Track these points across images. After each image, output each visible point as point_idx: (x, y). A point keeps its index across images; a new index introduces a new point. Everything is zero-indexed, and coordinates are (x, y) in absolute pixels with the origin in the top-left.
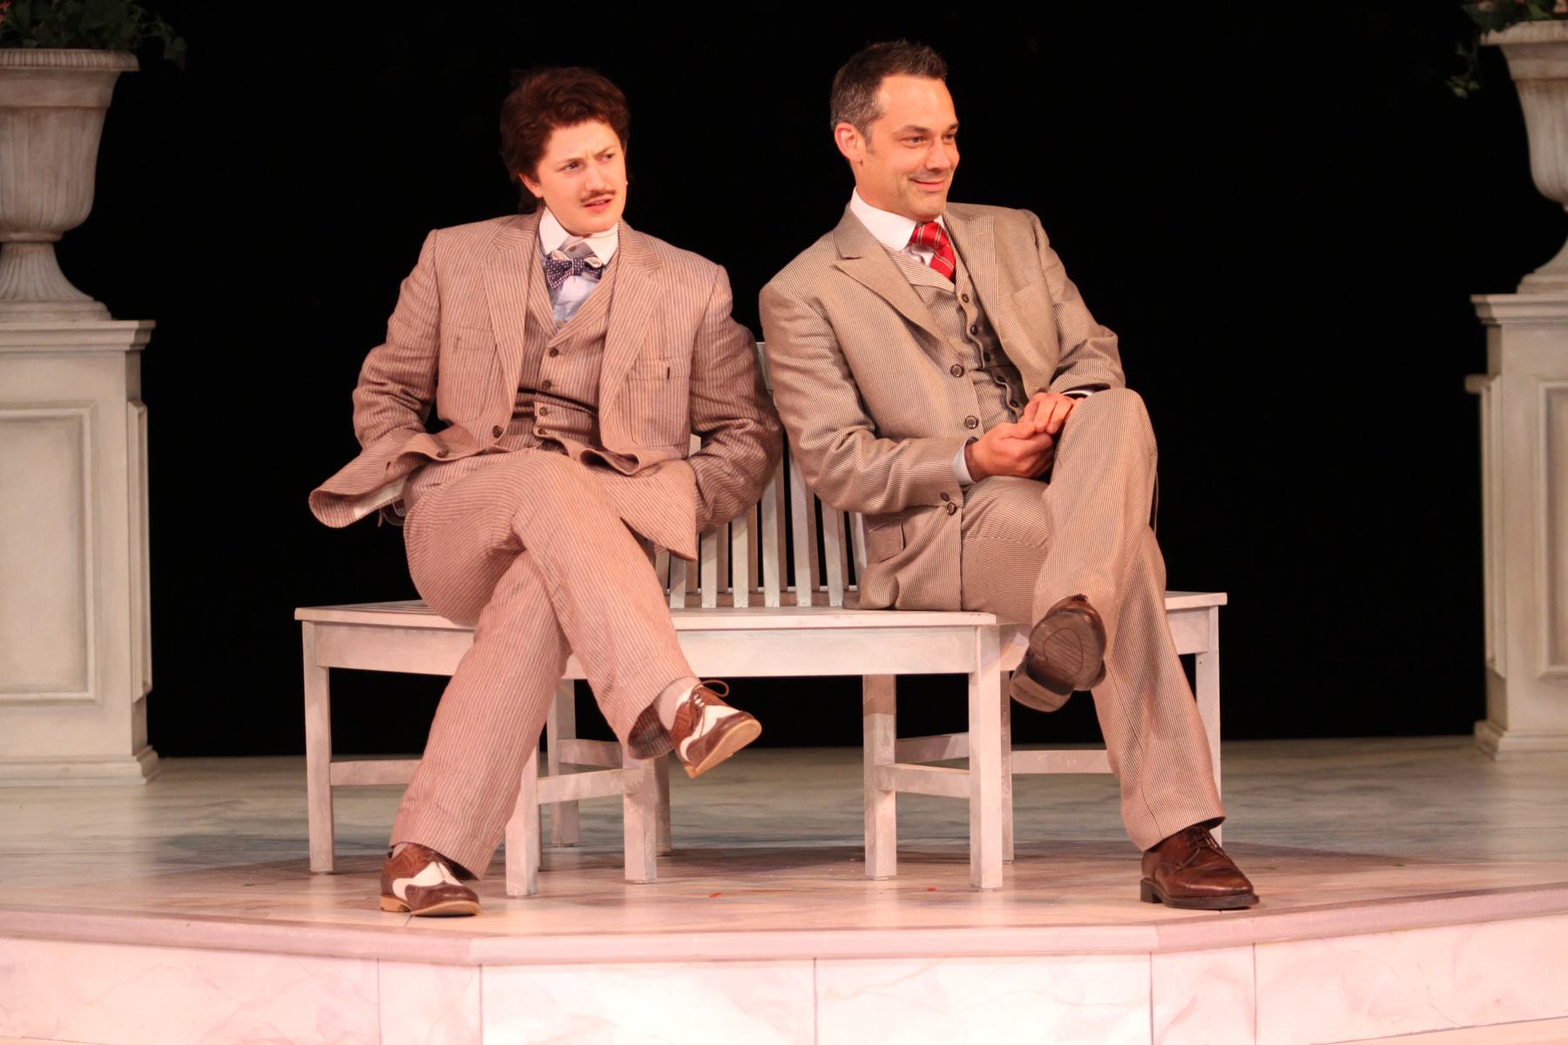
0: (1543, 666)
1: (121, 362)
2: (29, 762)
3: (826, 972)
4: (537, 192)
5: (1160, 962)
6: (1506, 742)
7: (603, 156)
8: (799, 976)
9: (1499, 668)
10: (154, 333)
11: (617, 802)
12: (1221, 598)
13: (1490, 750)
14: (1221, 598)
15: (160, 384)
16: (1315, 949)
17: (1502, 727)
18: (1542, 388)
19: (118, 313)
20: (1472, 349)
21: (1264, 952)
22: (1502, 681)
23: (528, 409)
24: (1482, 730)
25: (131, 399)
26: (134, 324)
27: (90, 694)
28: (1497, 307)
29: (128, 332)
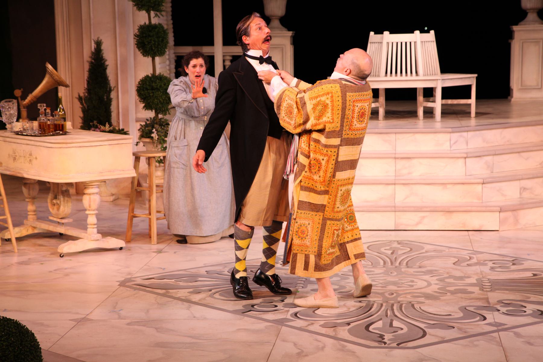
0: (520, 87)
1: (289, 38)
3: (398, 135)
4: (187, 71)
5: (452, 134)
6: (513, 100)
7: (201, 66)
8: (393, 136)
9: (512, 87)
10: (295, 34)
11: (378, 108)
12: (476, 75)
13: (510, 101)
14: (476, 75)
15: (295, 42)
16: (478, 132)
17: (512, 97)
18: (521, 41)
19: (289, 30)
20: (510, 35)
21: (469, 133)
22: (512, 90)
23: (58, 129)
24: (509, 98)
25: (291, 44)
26: (291, 32)
28: (515, 28)
29: (290, 33)
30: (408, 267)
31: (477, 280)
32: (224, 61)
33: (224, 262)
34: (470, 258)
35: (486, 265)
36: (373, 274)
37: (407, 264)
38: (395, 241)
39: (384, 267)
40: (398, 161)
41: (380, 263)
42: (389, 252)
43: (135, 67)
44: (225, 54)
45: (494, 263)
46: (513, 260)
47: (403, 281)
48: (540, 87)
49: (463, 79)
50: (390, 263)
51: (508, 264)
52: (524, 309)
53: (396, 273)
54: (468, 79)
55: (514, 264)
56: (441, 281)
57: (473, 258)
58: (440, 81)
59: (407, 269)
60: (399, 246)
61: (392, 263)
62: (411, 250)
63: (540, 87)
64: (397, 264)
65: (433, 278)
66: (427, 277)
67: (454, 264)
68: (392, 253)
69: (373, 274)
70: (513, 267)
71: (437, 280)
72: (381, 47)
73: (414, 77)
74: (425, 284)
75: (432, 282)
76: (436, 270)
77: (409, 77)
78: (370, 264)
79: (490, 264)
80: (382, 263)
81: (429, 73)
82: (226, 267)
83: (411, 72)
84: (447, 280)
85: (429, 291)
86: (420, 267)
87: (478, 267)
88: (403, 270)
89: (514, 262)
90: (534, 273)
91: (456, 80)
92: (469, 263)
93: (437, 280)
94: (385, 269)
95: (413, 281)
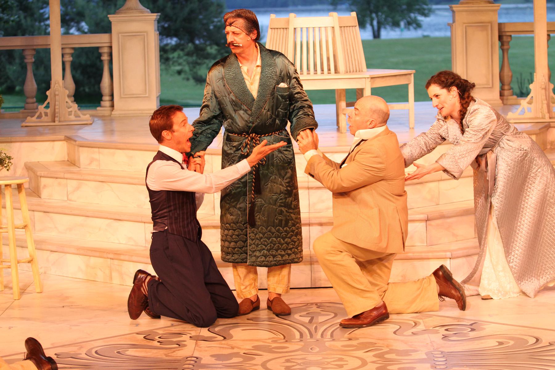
2: (134, 110)
10: (160, 16)
19: (152, 12)
27: (147, 95)
29: (155, 16)
30: (334, 340)
31: (427, 354)
32: (63, 56)
33: (80, 341)
34: (416, 324)
35: (437, 332)
36: (286, 352)
37: (332, 335)
38: (312, 304)
39: (301, 341)
40: (312, 191)
41: (295, 335)
42: (307, 320)
43: (466, 11)
44: (64, 46)
45: (447, 330)
46: (471, 325)
47: (329, 360)
48: (491, 86)
49: (398, 77)
50: (308, 335)
51: (465, 330)
52: (160, 340)
53: (318, 349)
54: (404, 77)
55: (473, 330)
56: (379, 357)
57: (420, 323)
58: (364, 79)
59: (333, 343)
60: (318, 310)
61: (311, 336)
62: (537, 340)
63: (491, 86)
64: (319, 336)
65: (368, 353)
66: (360, 353)
67: (395, 333)
68: (311, 321)
69: (286, 352)
70: (472, 334)
71: (375, 356)
72: (287, 34)
73: (333, 76)
74: (359, 363)
75: (368, 360)
76: (371, 343)
77: (326, 76)
78: (282, 337)
79: (442, 331)
80: (297, 335)
81: (351, 70)
82: (82, 347)
83: (322, 70)
84: (387, 356)
85: (267, 356)
86: (350, 339)
87: (426, 336)
88: (327, 344)
89: (472, 327)
90: (500, 340)
91: (388, 78)
92: (414, 330)
93: (375, 356)
94: (302, 343)
95: (341, 360)
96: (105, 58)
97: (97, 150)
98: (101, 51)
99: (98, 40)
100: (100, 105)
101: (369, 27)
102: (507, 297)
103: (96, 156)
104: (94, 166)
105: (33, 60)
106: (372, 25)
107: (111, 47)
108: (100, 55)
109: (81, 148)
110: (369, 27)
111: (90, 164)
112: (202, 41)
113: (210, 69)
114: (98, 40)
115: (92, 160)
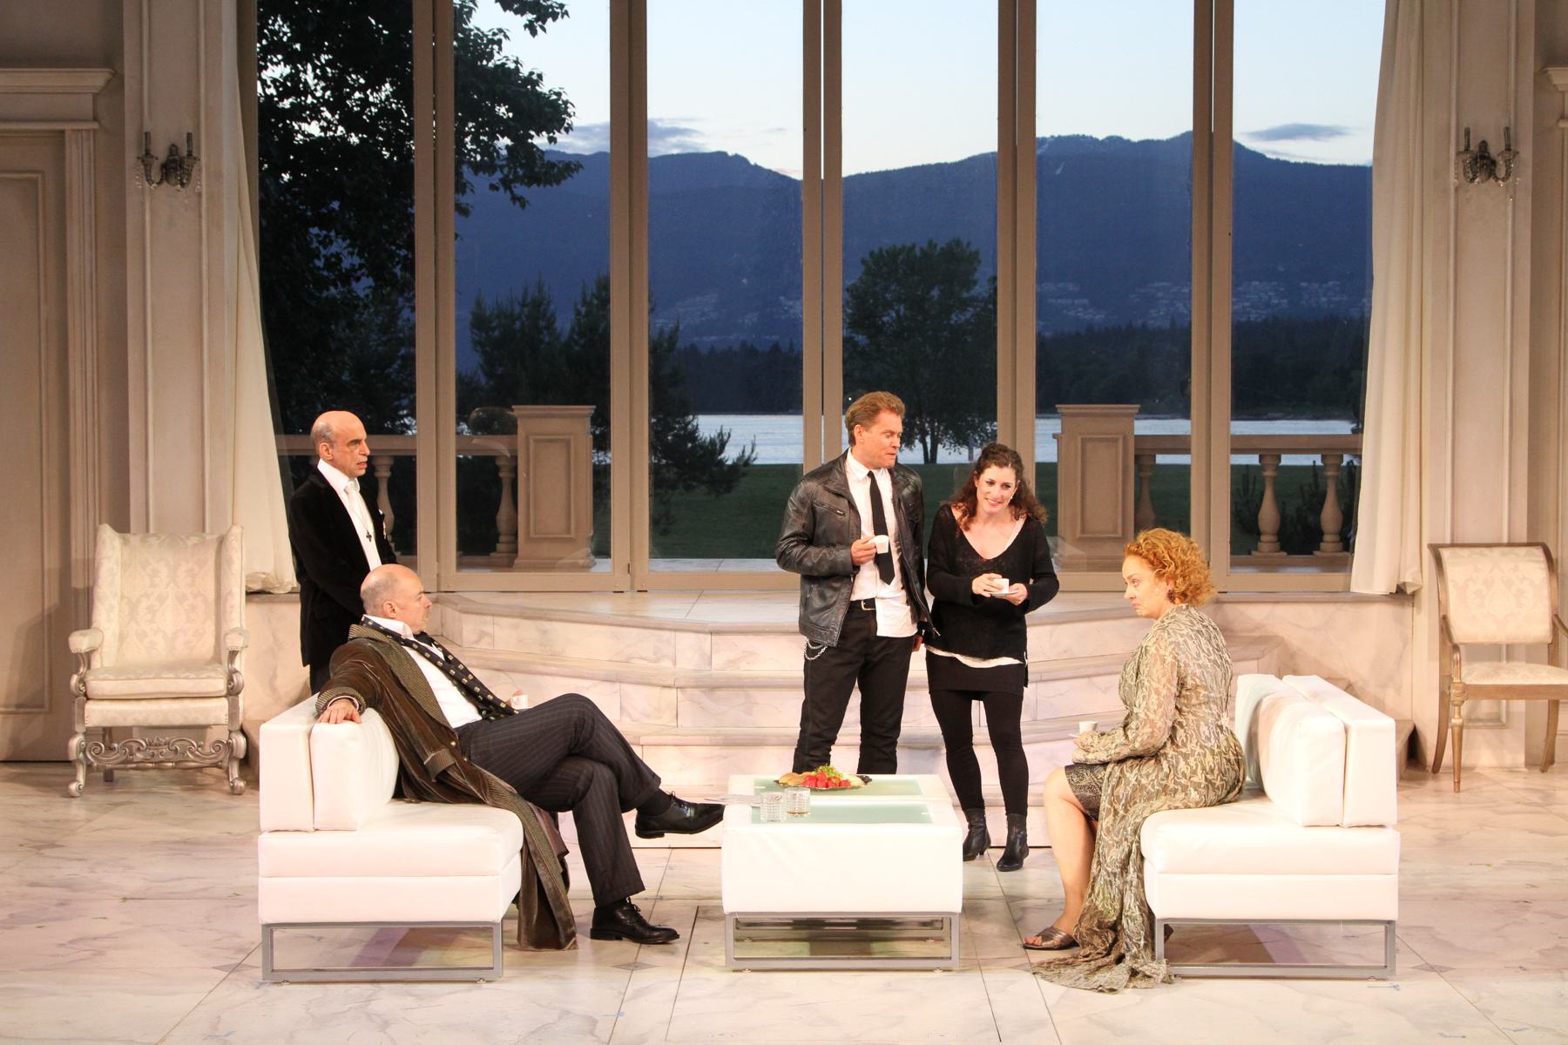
27: (572, 535)
48: (1120, 534)
96: (504, 475)
97: (489, 618)
98: (499, 463)
99: (497, 445)
100: (494, 550)
101: (918, 445)
102: (330, 134)
103: (489, 629)
104: (484, 645)
105: (363, 472)
106: (923, 442)
107: (515, 458)
108: (497, 469)
109: (464, 616)
110: (918, 445)
111: (477, 642)
112: (867, 585)
113: (892, 410)
114: (497, 445)
115: (482, 635)
